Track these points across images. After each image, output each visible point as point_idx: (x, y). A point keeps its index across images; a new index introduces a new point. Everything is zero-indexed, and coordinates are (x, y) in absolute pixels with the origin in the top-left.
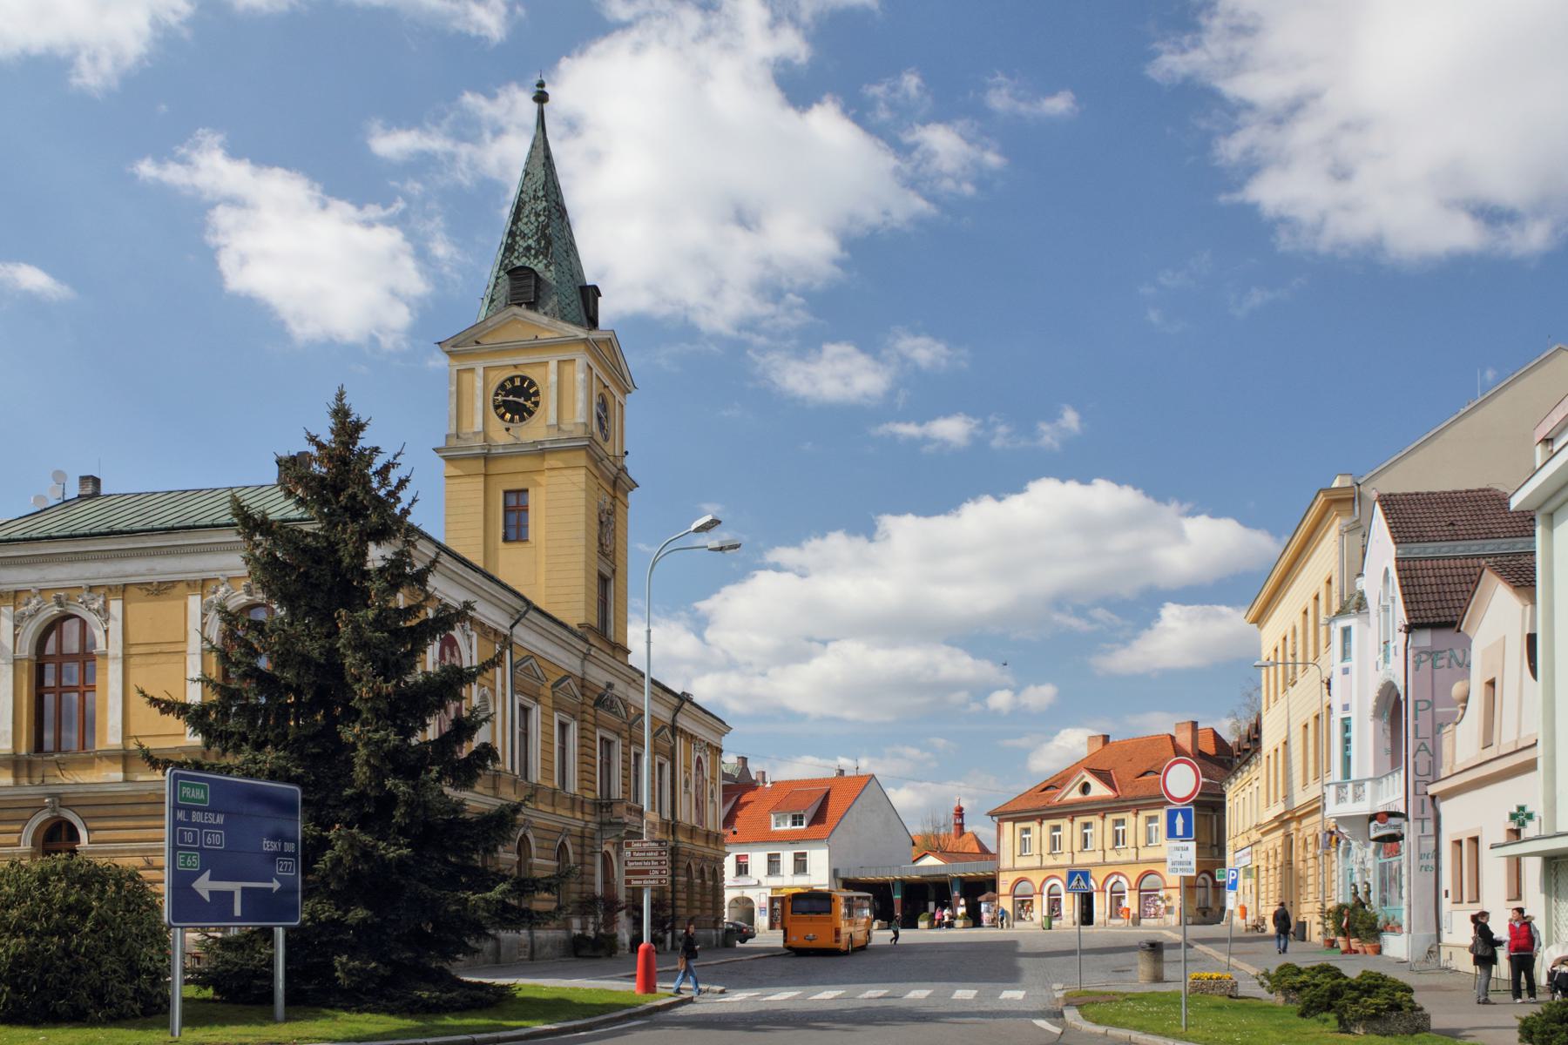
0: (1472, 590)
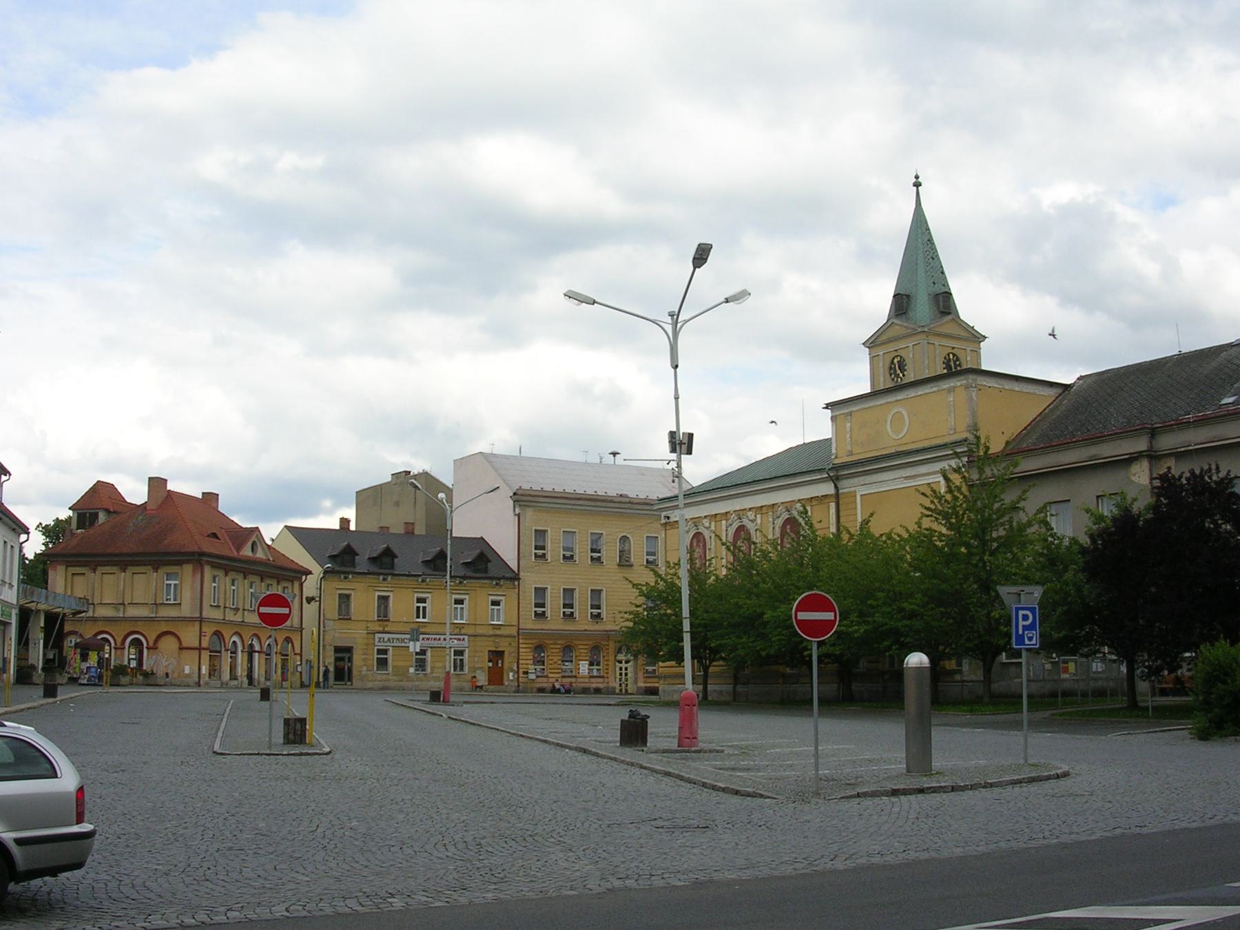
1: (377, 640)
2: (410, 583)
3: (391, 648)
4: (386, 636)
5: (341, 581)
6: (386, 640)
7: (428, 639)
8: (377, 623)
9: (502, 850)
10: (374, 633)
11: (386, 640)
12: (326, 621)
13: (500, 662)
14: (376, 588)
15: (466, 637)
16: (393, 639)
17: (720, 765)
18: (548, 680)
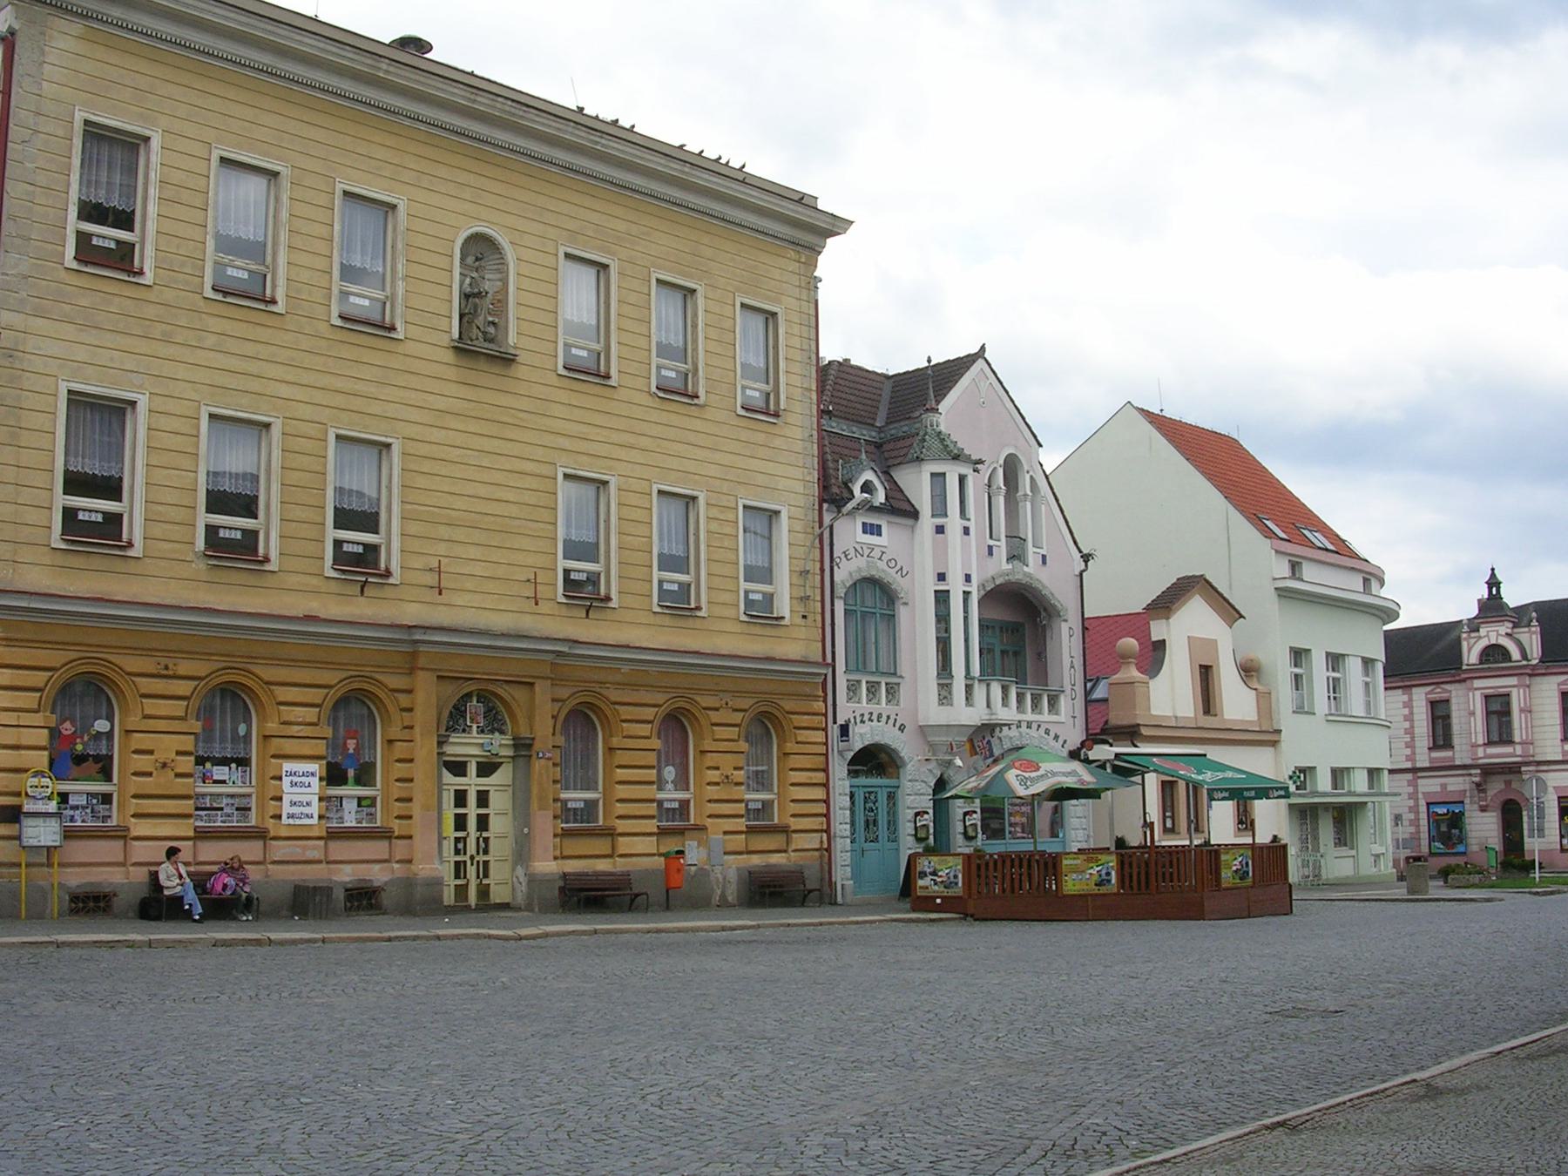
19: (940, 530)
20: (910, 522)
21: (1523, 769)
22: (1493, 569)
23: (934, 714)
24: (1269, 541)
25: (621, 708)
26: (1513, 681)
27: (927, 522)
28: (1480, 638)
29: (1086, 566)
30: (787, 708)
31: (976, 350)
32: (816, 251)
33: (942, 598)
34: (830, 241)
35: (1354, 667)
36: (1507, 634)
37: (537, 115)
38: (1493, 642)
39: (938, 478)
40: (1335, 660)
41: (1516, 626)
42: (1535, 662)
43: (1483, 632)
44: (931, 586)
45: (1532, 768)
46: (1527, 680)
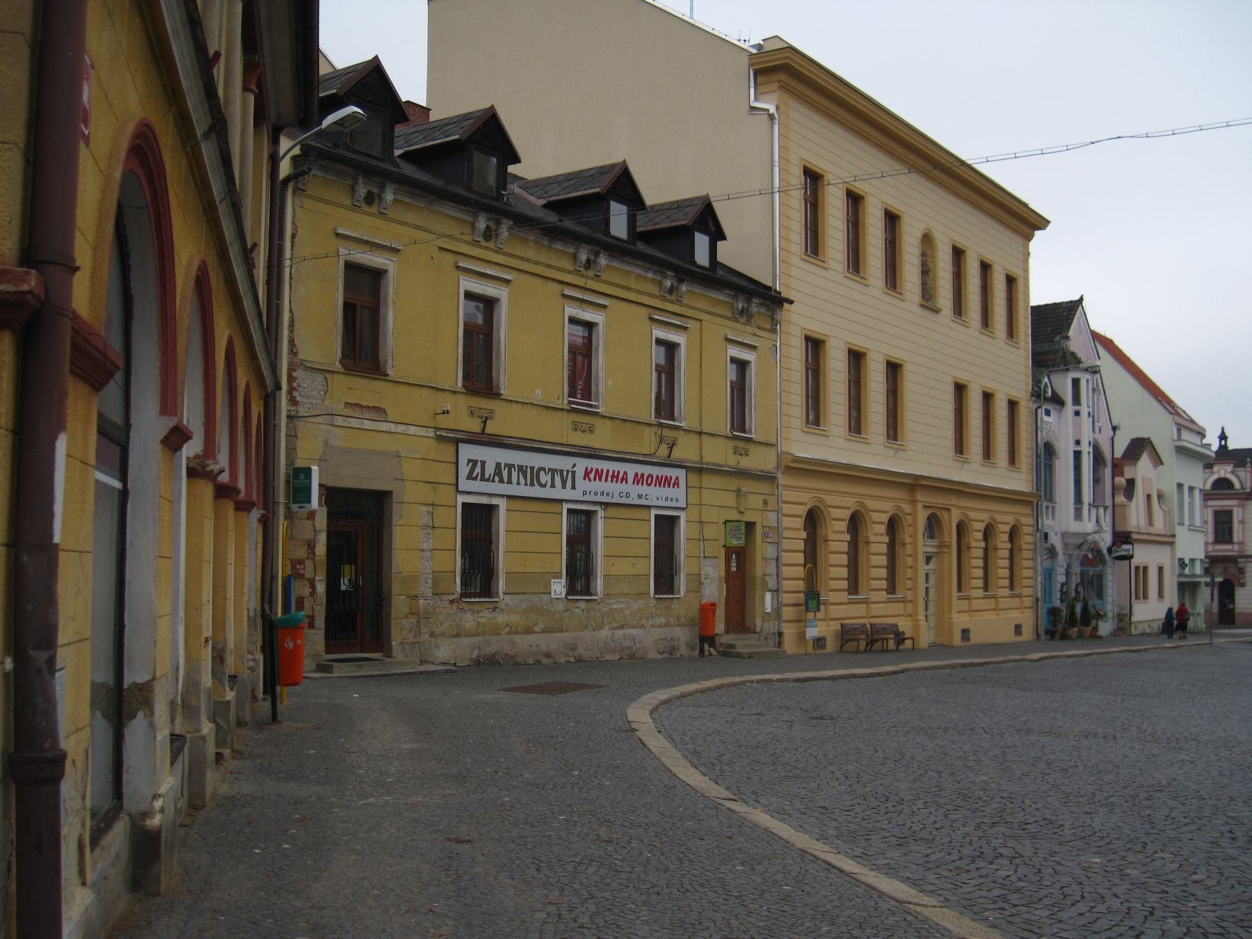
0: (588, 426)
1: (464, 470)
2: (632, 284)
3: (502, 504)
4: (492, 456)
5: (355, 208)
6: (490, 470)
7: (599, 474)
8: (568, 419)
9: (1215, 908)
10: (457, 442)
11: (490, 470)
12: (298, 373)
13: (734, 569)
14: (568, 292)
15: (681, 474)
16: (510, 467)
17: (1095, 858)
18: (970, 605)
19: (1077, 413)
20: (1058, 407)
21: (1239, 560)
22: (1223, 429)
23: (1074, 527)
24: (1172, 416)
25: (872, 514)
26: (1235, 502)
27: (1070, 408)
28: (1213, 473)
29: (1114, 433)
30: (870, 507)
31: (1077, 298)
32: (1029, 238)
33: (1077, 455)
34: (1038, 234)
35: (1197, 493)
36: (1232, 472)
37: (862, 130)
38: (1222, 476)
39: (1076, 382)
40: (1191, 489)
41: (1235, 466)
42: (1248, 490)
43: (1215, 469)
44: (1072, 448)
45: (1244, 560)
46: (1243, 502)
